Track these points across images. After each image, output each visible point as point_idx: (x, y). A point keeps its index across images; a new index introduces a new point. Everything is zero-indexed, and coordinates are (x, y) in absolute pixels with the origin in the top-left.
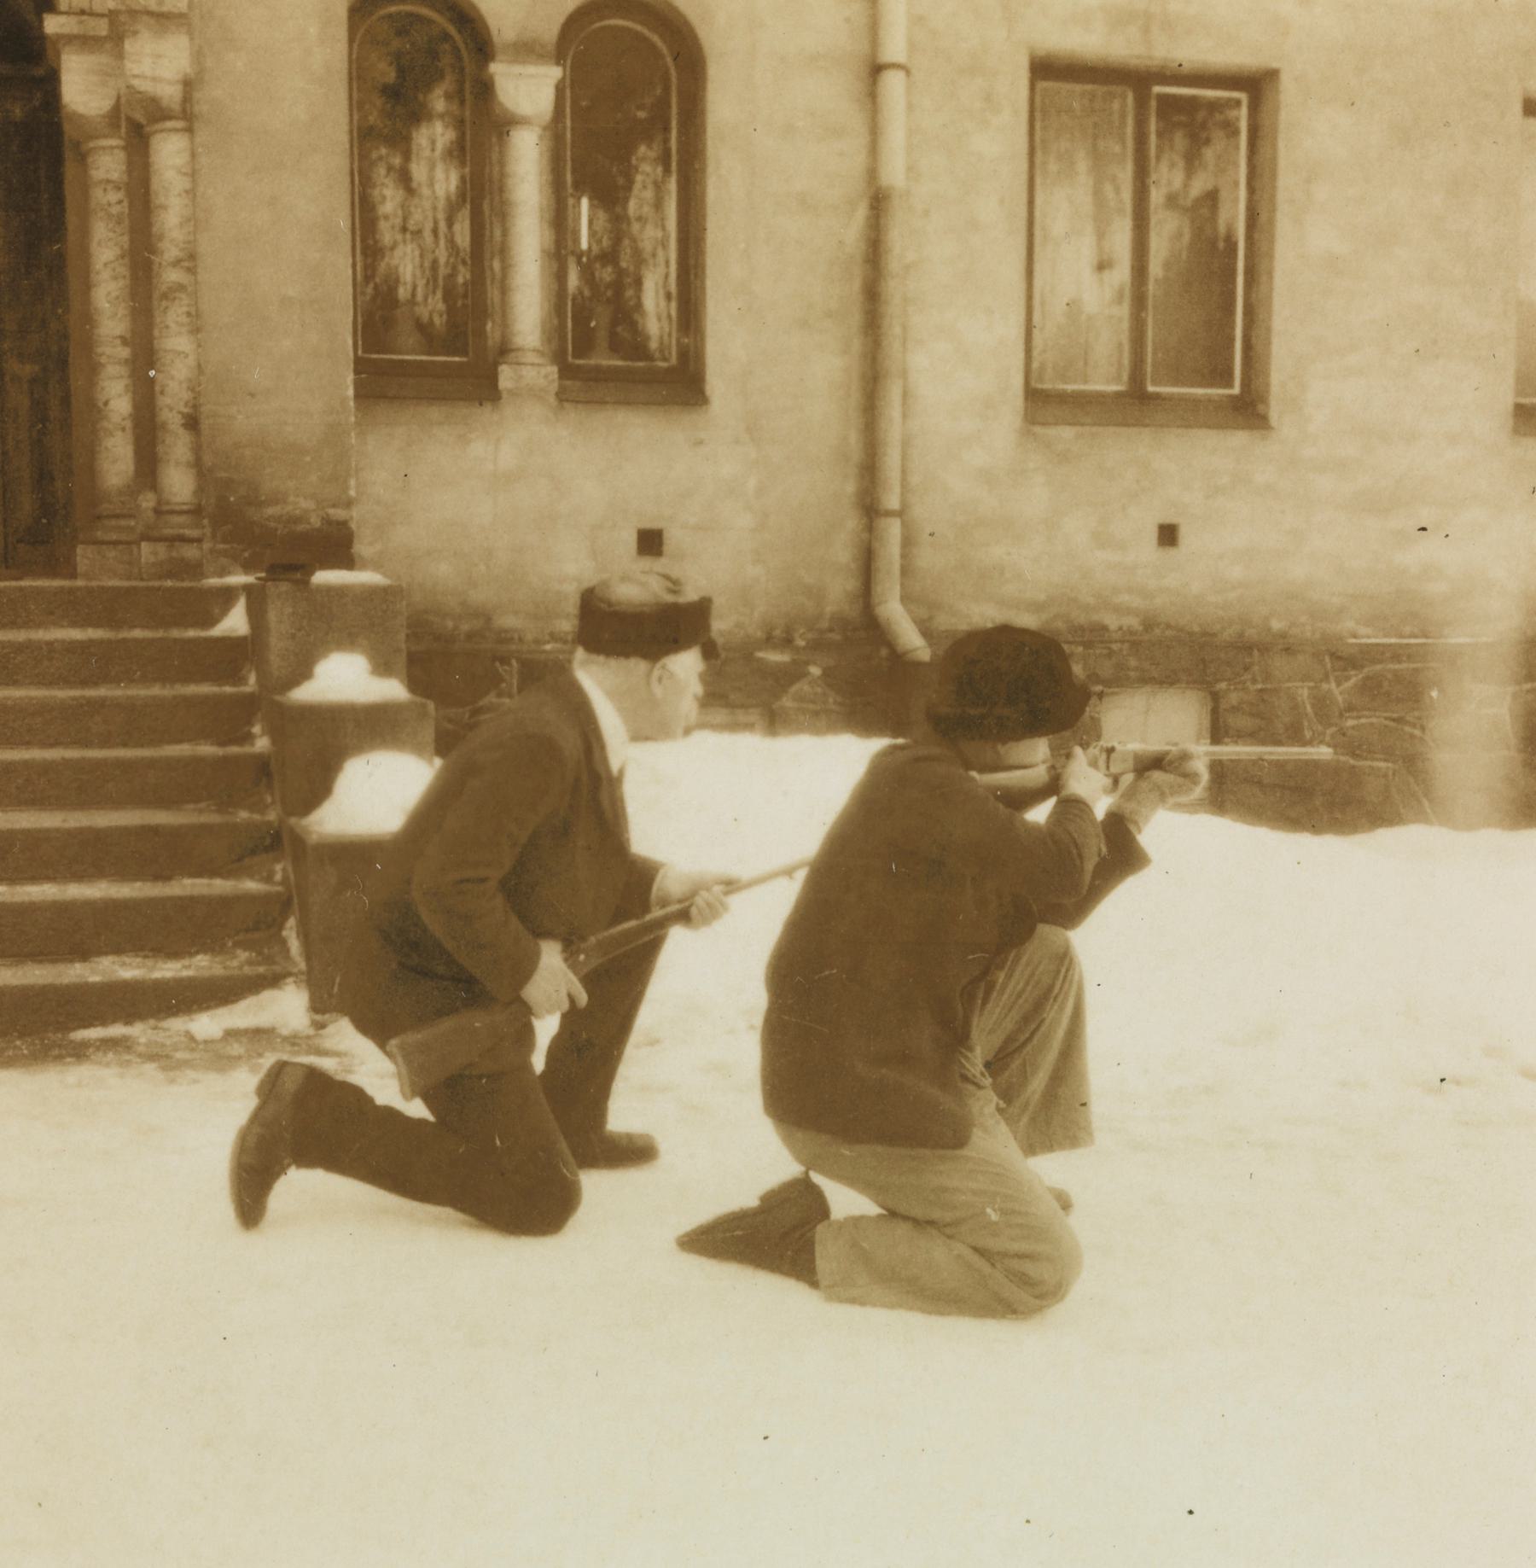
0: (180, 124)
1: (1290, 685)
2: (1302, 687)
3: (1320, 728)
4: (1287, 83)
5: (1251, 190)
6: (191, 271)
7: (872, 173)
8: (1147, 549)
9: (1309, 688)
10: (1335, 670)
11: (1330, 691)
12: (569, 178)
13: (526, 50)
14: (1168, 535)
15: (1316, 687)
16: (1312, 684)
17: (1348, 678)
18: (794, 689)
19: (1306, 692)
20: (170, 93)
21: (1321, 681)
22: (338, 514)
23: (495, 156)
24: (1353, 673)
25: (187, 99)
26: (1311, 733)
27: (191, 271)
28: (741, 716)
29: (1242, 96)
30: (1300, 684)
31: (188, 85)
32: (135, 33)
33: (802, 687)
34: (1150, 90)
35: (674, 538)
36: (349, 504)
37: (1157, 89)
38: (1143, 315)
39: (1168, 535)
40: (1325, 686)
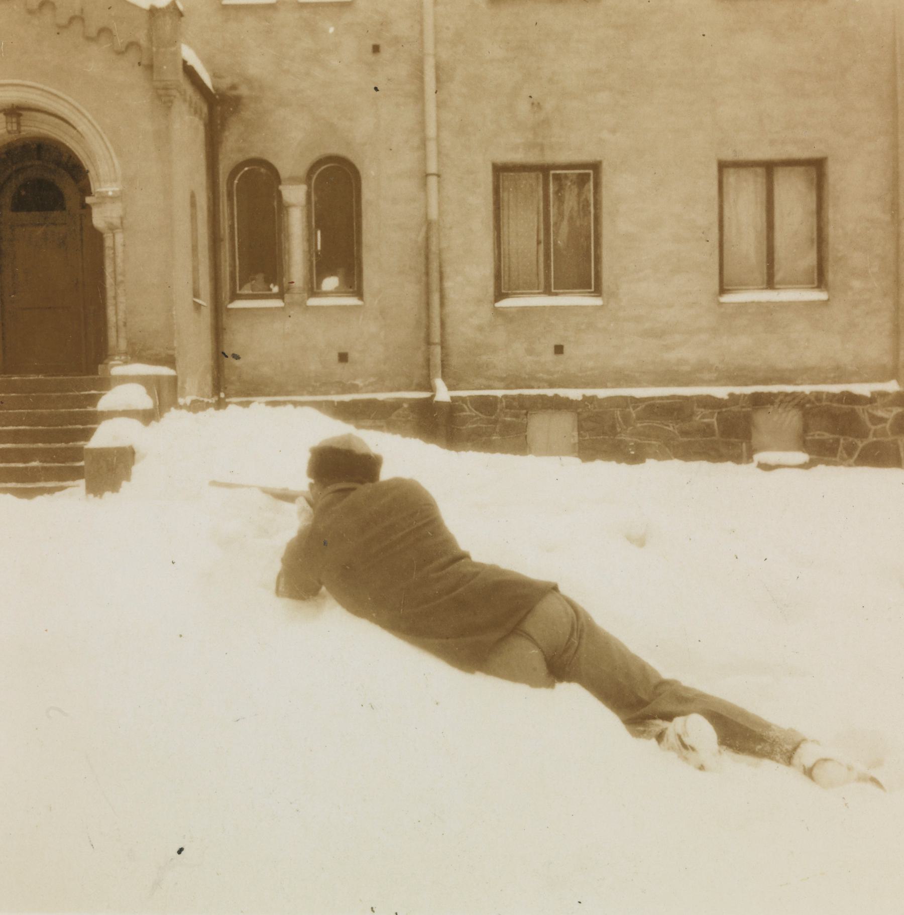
0: (121, 230)
1: (612, 409)
2: (617, 410)
3: (625, 427)
4: (605, 165)
5: (596, 208)
6: (124, 276)
7: (426, 214)
8: (549, 356)
9: (620, 411)
10: (632, 403)
11: (630, 412)
12: (313, 223)
13: (294, 180)
14: (559, 349)
15: (622, 411)
16: (621, 409)
17: (638, 407)
18: (396, 413)
19: (618, 413)
20: (117, 222)
21: (625, 408)
22: (170, 352)
23: (285, 219)
24: (640, 404)
25: (122, 223)
26: (620, 429)
27: (124, 276)
28: (378, 423)
29: (591, 172)
30: (616, 409)
31: (122, 219)
32: (106, 203)
33: (400, 411)
34: (549, 173)
35: (353, 355)
36: (174, 349)
37: (552, 172)
38: (549, 262)
39: (559, 349)
40: (628, 410)
